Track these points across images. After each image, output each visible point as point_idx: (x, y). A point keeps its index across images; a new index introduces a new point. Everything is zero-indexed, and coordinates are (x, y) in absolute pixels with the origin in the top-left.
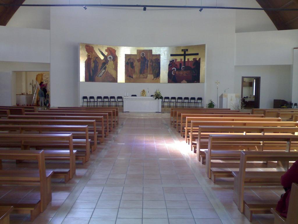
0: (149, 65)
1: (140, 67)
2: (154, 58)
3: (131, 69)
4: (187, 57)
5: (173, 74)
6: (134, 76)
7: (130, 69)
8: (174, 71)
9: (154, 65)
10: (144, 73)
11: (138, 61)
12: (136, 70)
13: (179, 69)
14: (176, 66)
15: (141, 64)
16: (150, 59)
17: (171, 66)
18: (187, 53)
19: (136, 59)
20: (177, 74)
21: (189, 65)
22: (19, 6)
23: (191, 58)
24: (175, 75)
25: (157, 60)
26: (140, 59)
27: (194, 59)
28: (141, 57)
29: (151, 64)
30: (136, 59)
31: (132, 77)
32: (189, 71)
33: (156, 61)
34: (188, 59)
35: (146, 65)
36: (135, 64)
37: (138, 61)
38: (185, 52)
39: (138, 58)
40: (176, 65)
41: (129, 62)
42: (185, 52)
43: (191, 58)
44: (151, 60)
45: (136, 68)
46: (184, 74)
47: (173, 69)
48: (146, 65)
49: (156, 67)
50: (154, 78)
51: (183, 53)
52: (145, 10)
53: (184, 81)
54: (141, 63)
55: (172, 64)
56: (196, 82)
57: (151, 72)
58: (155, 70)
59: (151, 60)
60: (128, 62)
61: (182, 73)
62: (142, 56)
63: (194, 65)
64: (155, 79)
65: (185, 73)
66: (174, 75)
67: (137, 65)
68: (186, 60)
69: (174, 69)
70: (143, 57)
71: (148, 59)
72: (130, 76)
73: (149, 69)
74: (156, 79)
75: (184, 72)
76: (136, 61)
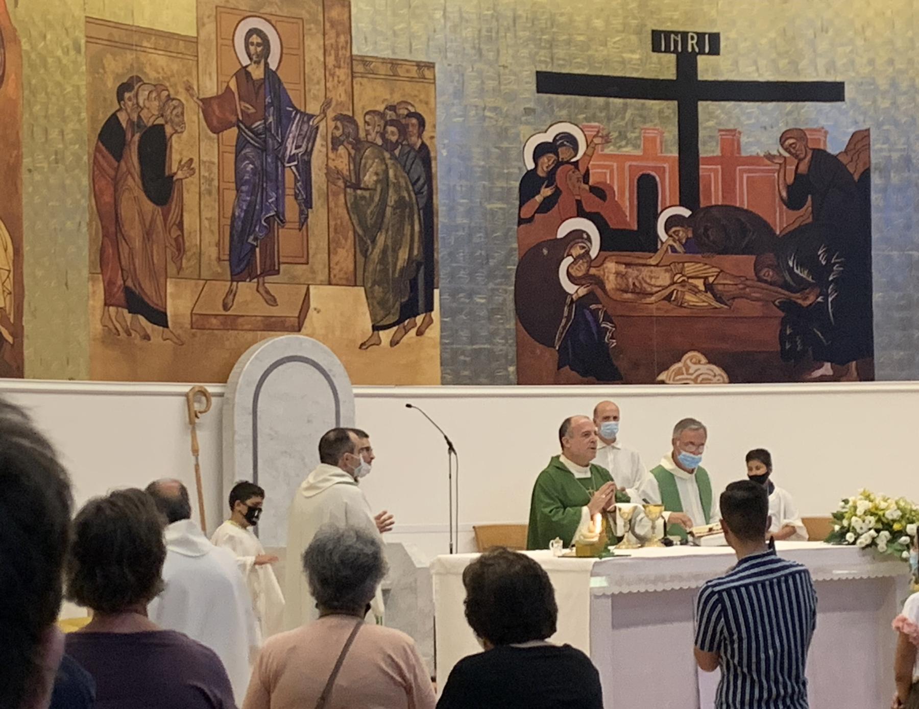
0: (318, 177)
1: (231, 196)
2: (372, 96)
3: (148, 206)
4: (713, 116)
5: (570, 288)
6: (178, 302)
7: (135, 204)
8: (577, 251)
9: (369, 178)
10: (272, 270)
11: (216, 113)
12: (189, 221)
13: (630, 241)
14: (594, 201)
15: (239, 157)
16: (327, 103)
17: (547, 205)
18: (708, 68)
19: (189, 89)
20: (611, 283)
21: (743, 200)
22: (468, 591)
23: (759, 129)
24: (590, 297)
25: (403, 131)
26: (225, 96)
27: (793, 138)
28: (243, 74)
29: (342, 161)
30: (189, 89)
31: (159, 318)
32: (746, 262)
33: (392, 133)
34: (730, 139)
35: (290, 175)
36: (179, 150)
37: (216, 113)
38: (686, 63)
39: (210, 88)
40: (600, 192)
41: (123, 118)
42: (686, 63)
43: (759, 129)
44: (339, 118)
45: (190, 197)
46: (695, 291)
47: (562, 232)
48: (290, 175)
49: (392, 198)
50: (376, 328)
51: (664, 67)
52: (539, 90)
53: (694, 362)
54: (241, 144)
55: (552, 174)
56: (827, 369)
57: (345, 258)
58: (381, 239)
59: (339, 118)
60: (113, 120)
61: (663, 278)
62: (245, 61)
63: (793, 201)
64: (385, 336)
65: (700, 283)
66: (582, 303)
67: (202, 156)
68: (708, 148)
69: (577, 235)
70: (257, 73)
71: (313, 108)
72: (135, 303)
73: (318, 216)
74: (394, 343)
75: (690, 268)
76: (194, 118)
